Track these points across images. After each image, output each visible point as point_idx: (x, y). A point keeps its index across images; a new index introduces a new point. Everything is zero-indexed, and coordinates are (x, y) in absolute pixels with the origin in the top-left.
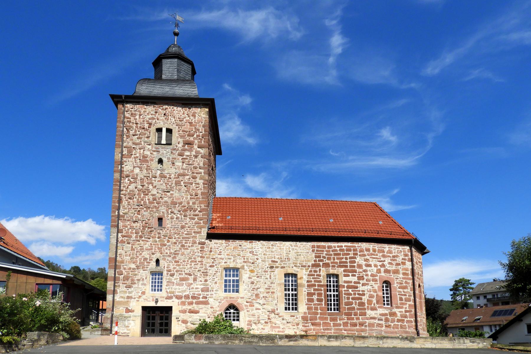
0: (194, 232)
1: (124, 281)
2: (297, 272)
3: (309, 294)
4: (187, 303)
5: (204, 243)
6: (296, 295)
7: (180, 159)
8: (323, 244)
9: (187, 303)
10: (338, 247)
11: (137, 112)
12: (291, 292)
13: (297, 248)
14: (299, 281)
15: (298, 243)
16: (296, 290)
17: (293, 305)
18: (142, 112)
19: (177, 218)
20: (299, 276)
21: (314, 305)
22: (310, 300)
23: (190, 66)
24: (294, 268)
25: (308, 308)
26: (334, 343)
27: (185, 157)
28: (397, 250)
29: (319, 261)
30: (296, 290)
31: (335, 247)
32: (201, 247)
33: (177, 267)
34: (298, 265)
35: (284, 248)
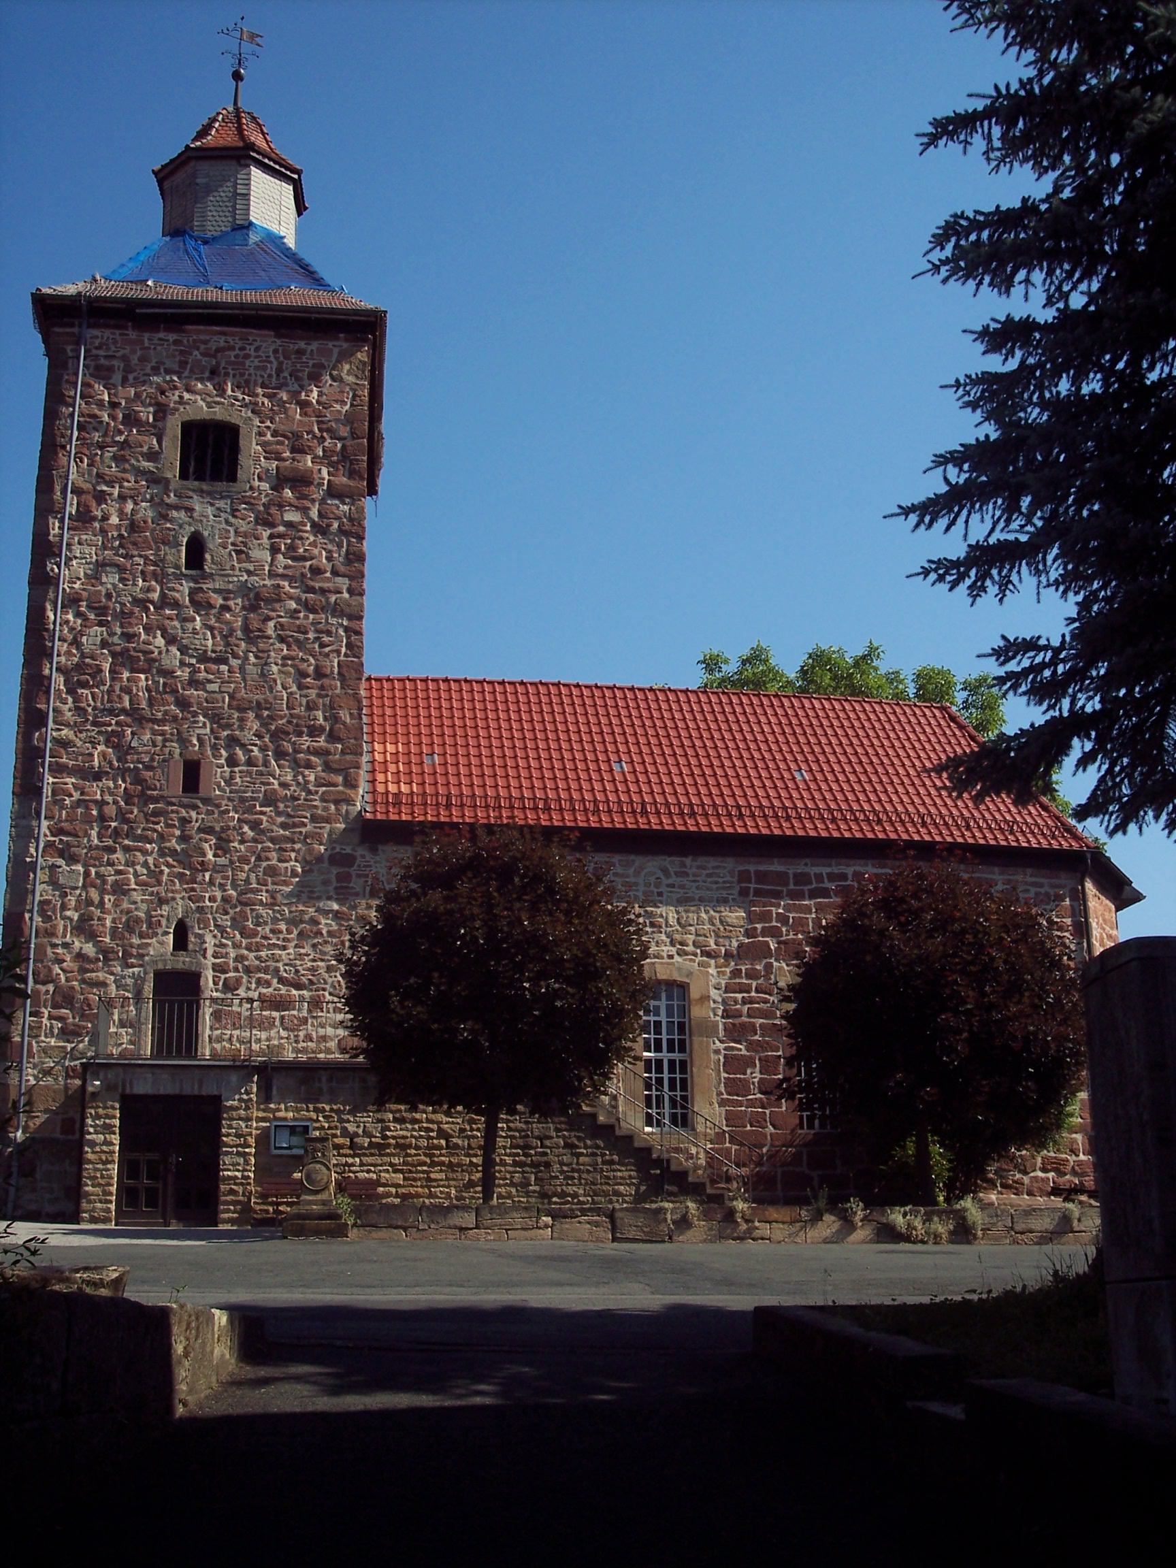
0: (314, 819)
1: (55, 1006)
2: (690, 974)
3: (733, 1063)
4: (850, 877)
5: (348, 860)
6: (683, 1064)
7: (266, 534)
8: (776, 866)
9: (850, 877)
10: (832, 877)
11: (115, 363)
12: (665, 1055)
13: (684, 881)
14: (696, 1012)
15: (688, 861)
16: (682, 1049)
17: (672, 1087)
18: (135, 360)
19: (250, 762)
20: (695, 993)
21: (751, 1104)
22: (735, 1087)
23: (288, 189)
24: (677, 958)
25: (730, 1118)
26: (206, 311)
27: (281, 529)
28: (1033, 890)
29: (765, 932)
30: (682, 1049)
31: (819, 877)
32: (340, 877)
33: (252, 955)
34: (690, 948)
35: (640, 880)
